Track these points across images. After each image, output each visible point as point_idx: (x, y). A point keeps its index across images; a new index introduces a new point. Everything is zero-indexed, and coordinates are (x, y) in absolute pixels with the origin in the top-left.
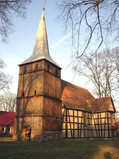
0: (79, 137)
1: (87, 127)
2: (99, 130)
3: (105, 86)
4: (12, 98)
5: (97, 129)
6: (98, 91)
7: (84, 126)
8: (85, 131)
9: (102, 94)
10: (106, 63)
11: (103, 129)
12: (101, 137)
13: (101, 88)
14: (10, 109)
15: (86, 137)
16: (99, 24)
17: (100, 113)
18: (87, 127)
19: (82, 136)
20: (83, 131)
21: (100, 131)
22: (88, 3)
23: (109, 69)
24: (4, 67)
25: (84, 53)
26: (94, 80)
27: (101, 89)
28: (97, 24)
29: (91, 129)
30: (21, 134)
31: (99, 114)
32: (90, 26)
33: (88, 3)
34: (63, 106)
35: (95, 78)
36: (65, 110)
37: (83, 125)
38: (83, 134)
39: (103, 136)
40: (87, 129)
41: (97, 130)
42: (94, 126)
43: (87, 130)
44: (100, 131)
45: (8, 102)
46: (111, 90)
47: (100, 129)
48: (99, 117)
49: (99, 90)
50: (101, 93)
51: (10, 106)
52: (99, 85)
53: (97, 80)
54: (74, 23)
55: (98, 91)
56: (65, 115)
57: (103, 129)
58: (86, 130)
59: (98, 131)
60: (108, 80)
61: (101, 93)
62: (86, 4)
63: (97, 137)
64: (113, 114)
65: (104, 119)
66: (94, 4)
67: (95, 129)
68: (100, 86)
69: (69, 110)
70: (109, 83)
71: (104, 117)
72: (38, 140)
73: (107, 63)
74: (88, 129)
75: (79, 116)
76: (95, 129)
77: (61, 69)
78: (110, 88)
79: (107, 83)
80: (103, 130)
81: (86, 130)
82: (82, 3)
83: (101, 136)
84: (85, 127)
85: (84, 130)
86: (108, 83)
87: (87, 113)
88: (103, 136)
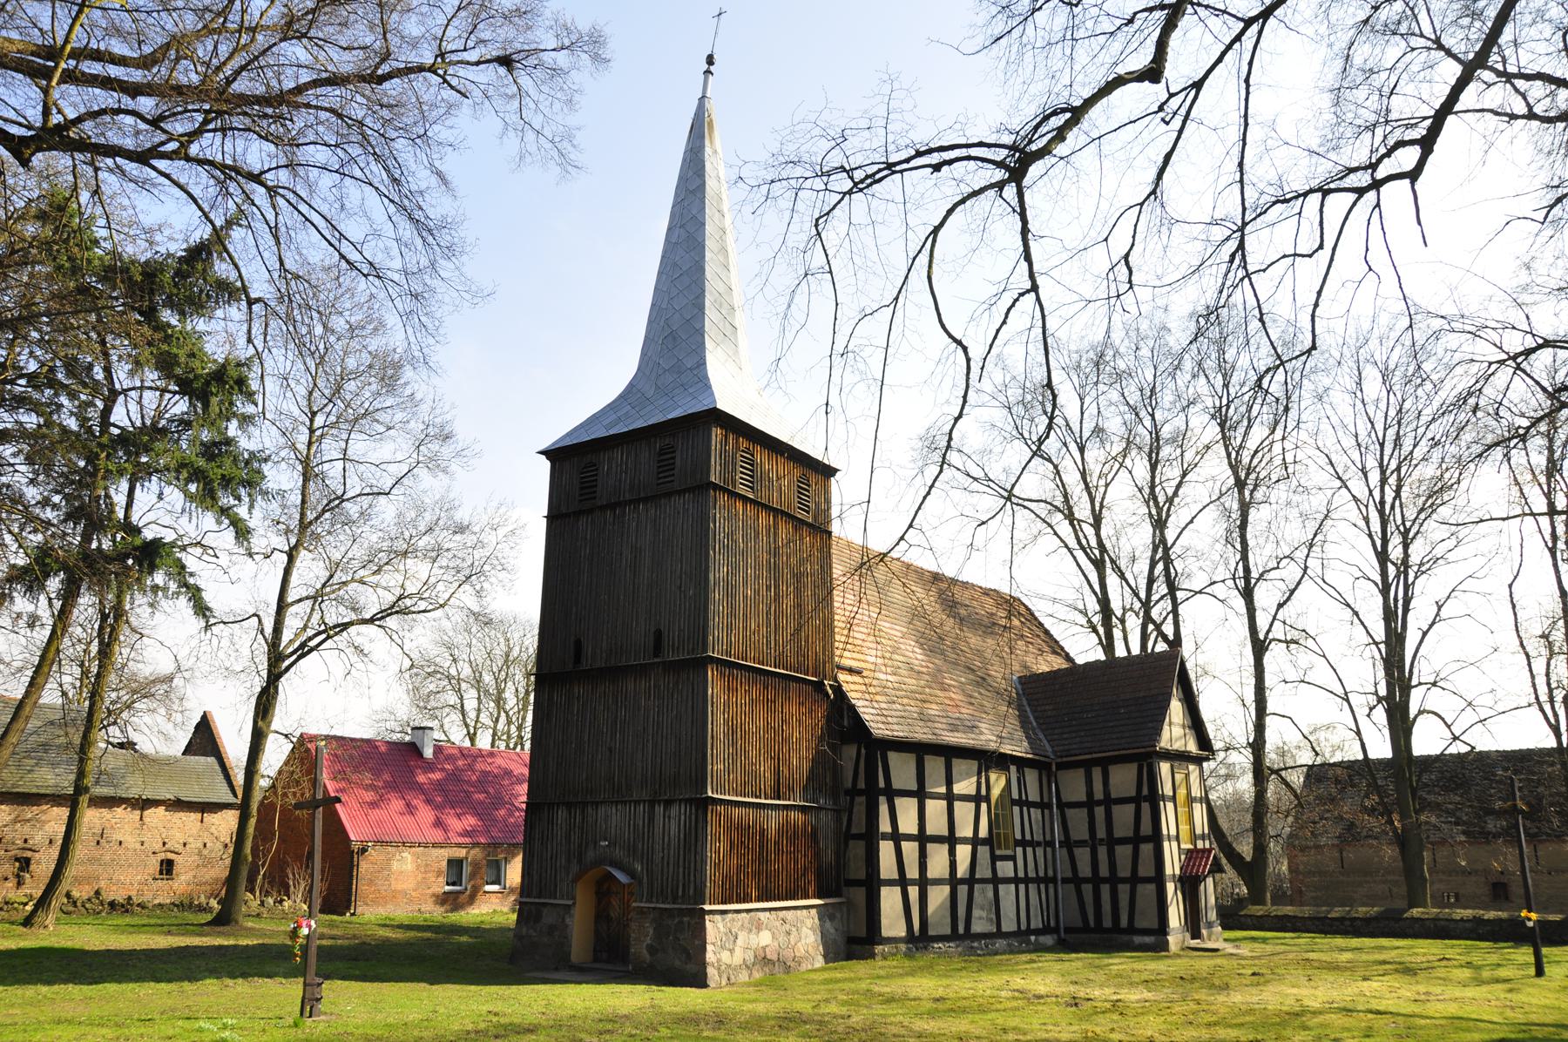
0: (961, 930)
1: (1011, 864)
2: (1096, 880)
3: (1143, 566)
4: (515, 653)
5: (1085, 870)
6: (1098, 608)
7: (994, 859)
8: (1001, 893)
9: (1123, 621)
10: (1143, 413)
11: (1124, 871)
12: (1108, 931)
13: (1112, 580)
14: (500, 726)
15: (1004, 929)
16: (1033, 294)
17: (1105, 764)
18: (1011, 864)
19: (977, 927)
20: (984, 893)
21: (1105, 890)
22: (950, 162)
23: (1166, 451)
24: (454, 467)
25: (911, 526)
26: (1065, 529)
27: (1118, 597)
28: (1022, 295)
29: (1041, 874)
30: (568, 920)
31: (1097, 773)
32: (959, 343)
33: (950, 162)
34: (846, 723)
35: (1070, 517)
36: (863, 751)
37: (984, 851)
38: (984, 914)
39: (1124, 922)
40: (1012, 874)
41: (1086, 880)
42: (1065, 850)
43: (1016, 880)
44: (1105, 890)
45: (488, 678)
46: (1180, 595)
47: (1104, 871)
48: (1099, 794)
49: (1104, 602)
50: (1119, 613)
51: (499, 701)
52: (1099, 565)
53: (1089, 531)
54: (848, 313)
55: (1093, 605)
56: (861, 785)
57: (1124, 871)
58: (1007, 881)
59: (1087, 889)
60: (1160, 524)
61: (1119, 613)
62: (937, 168)
63: (1086, 929)
64: (1191, 767)
65: (1131, 808)
66: (1000, 164)
67: (1069, 874)
68: (1109, 571)
69: (893, 757)
70: (1166, 550)
71: (1133, 793)
72: (677, 963)
73: (1153, 415)
74: (1021, 874)
75: (928, 832)
76: (1069, 874)
77: (829, 472)
78: (1172, 588)
79: (1155, 551)
80: (1124, 881)
81: (1007, 881)
82: (907, 161)
83: (1107, 922)
84: (999, 864)
85: (990, 887)
86: (1162, 550)
87: (1013, 768)
88: (1124, 922)
